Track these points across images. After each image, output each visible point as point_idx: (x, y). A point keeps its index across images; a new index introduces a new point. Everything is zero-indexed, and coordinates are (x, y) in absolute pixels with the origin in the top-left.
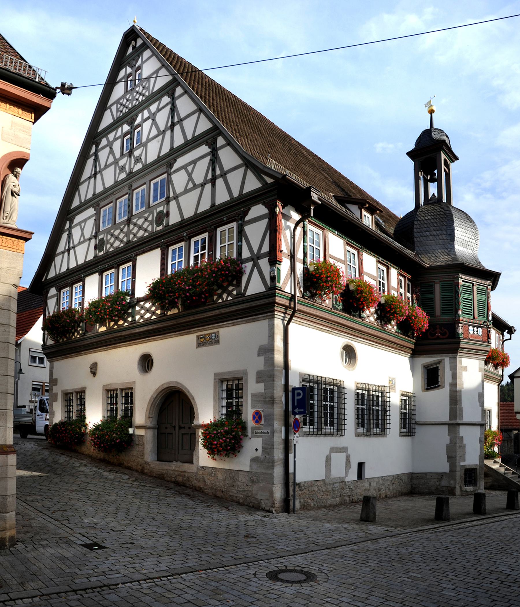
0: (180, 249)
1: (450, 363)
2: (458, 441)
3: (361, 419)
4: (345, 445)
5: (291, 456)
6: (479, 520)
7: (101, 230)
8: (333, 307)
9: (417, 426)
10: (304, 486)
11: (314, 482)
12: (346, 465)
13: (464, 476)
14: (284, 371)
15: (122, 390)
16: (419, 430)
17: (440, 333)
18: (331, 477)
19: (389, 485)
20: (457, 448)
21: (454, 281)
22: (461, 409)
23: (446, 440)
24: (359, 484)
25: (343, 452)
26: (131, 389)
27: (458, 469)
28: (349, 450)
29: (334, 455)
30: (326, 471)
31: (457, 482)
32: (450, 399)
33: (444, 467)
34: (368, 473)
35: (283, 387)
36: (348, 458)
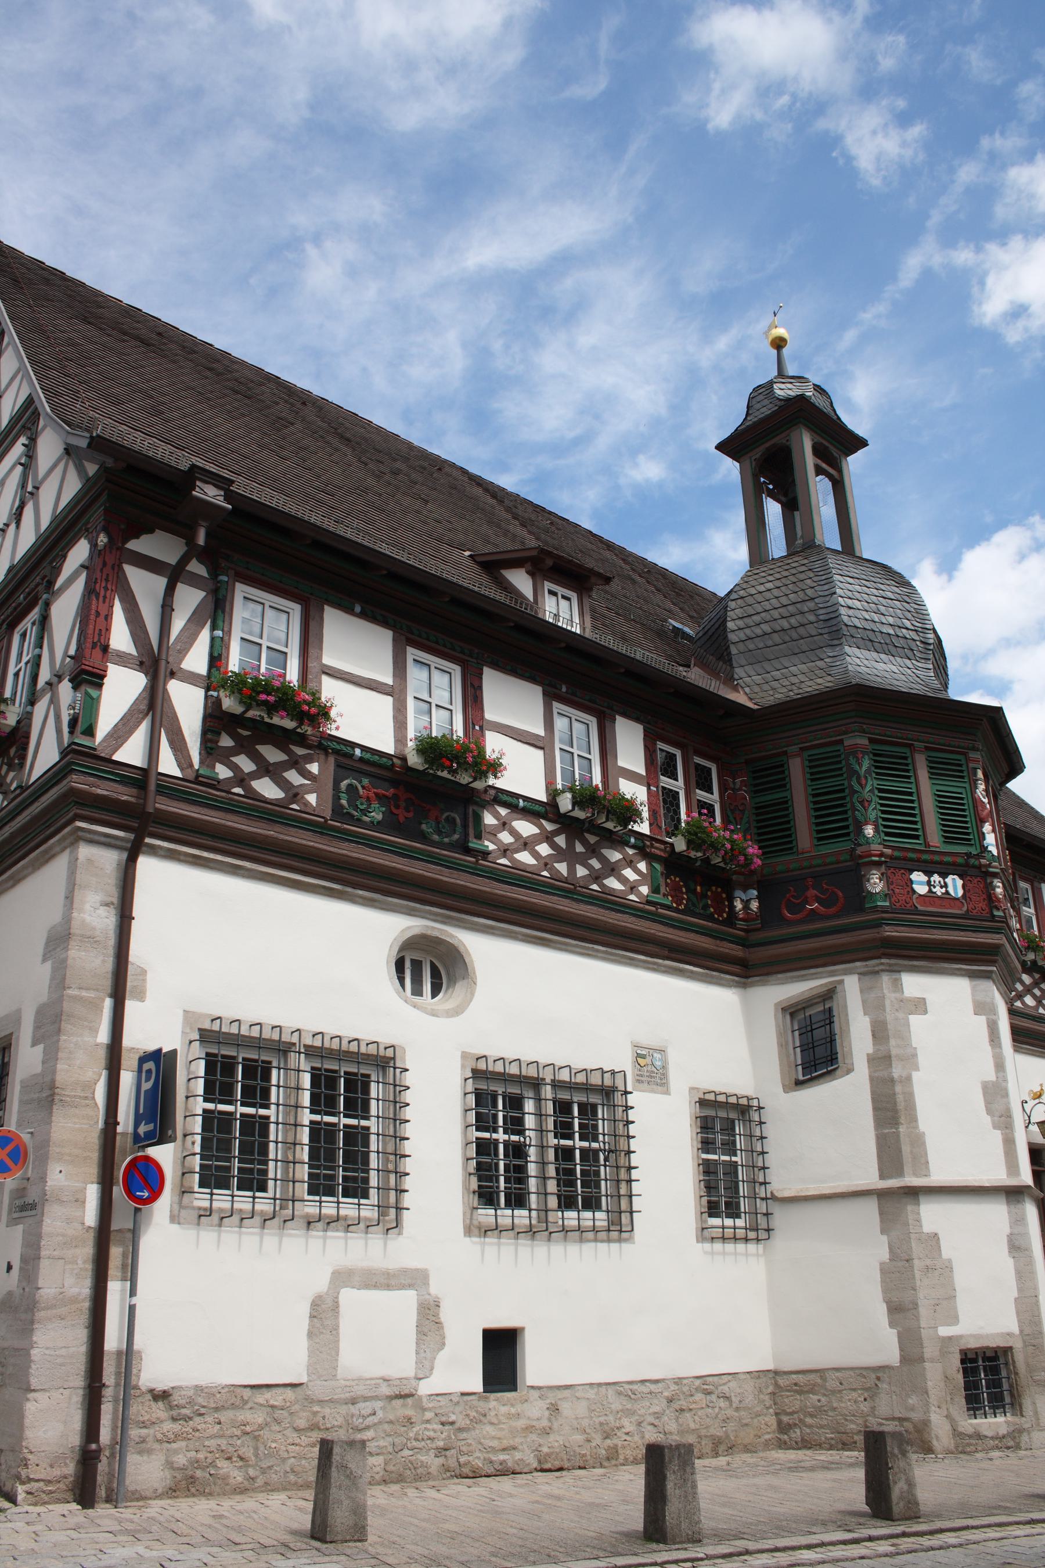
1: (861, 991)
2: (917, 1249)
3: (496, 1180)
5: (115, 1289)
6: (844, 1542)
8: (338, 811)
9: (775, 1208)
10: (191, 1402)
11: (247, 1393)
12: (421, 1333)
13: (960, 1378)
14: (108, 1003)
16: (781, 1217)
17: (818, 899)
18: (340, 1373)
19: (658, 1415)
20: (918, 1274)
21: (841, 742)
22: (919, 1141)
23: (880, 1250)
24: (500, 1403)
25: (410, 1286)
27: (930, 1350)
28: (432, 1282)
29: (348, 1297)
31: (933, 1399)
32: (875, 1109)
33: (883, 1346)
34: (536, 1365)
35: (102, 1054)
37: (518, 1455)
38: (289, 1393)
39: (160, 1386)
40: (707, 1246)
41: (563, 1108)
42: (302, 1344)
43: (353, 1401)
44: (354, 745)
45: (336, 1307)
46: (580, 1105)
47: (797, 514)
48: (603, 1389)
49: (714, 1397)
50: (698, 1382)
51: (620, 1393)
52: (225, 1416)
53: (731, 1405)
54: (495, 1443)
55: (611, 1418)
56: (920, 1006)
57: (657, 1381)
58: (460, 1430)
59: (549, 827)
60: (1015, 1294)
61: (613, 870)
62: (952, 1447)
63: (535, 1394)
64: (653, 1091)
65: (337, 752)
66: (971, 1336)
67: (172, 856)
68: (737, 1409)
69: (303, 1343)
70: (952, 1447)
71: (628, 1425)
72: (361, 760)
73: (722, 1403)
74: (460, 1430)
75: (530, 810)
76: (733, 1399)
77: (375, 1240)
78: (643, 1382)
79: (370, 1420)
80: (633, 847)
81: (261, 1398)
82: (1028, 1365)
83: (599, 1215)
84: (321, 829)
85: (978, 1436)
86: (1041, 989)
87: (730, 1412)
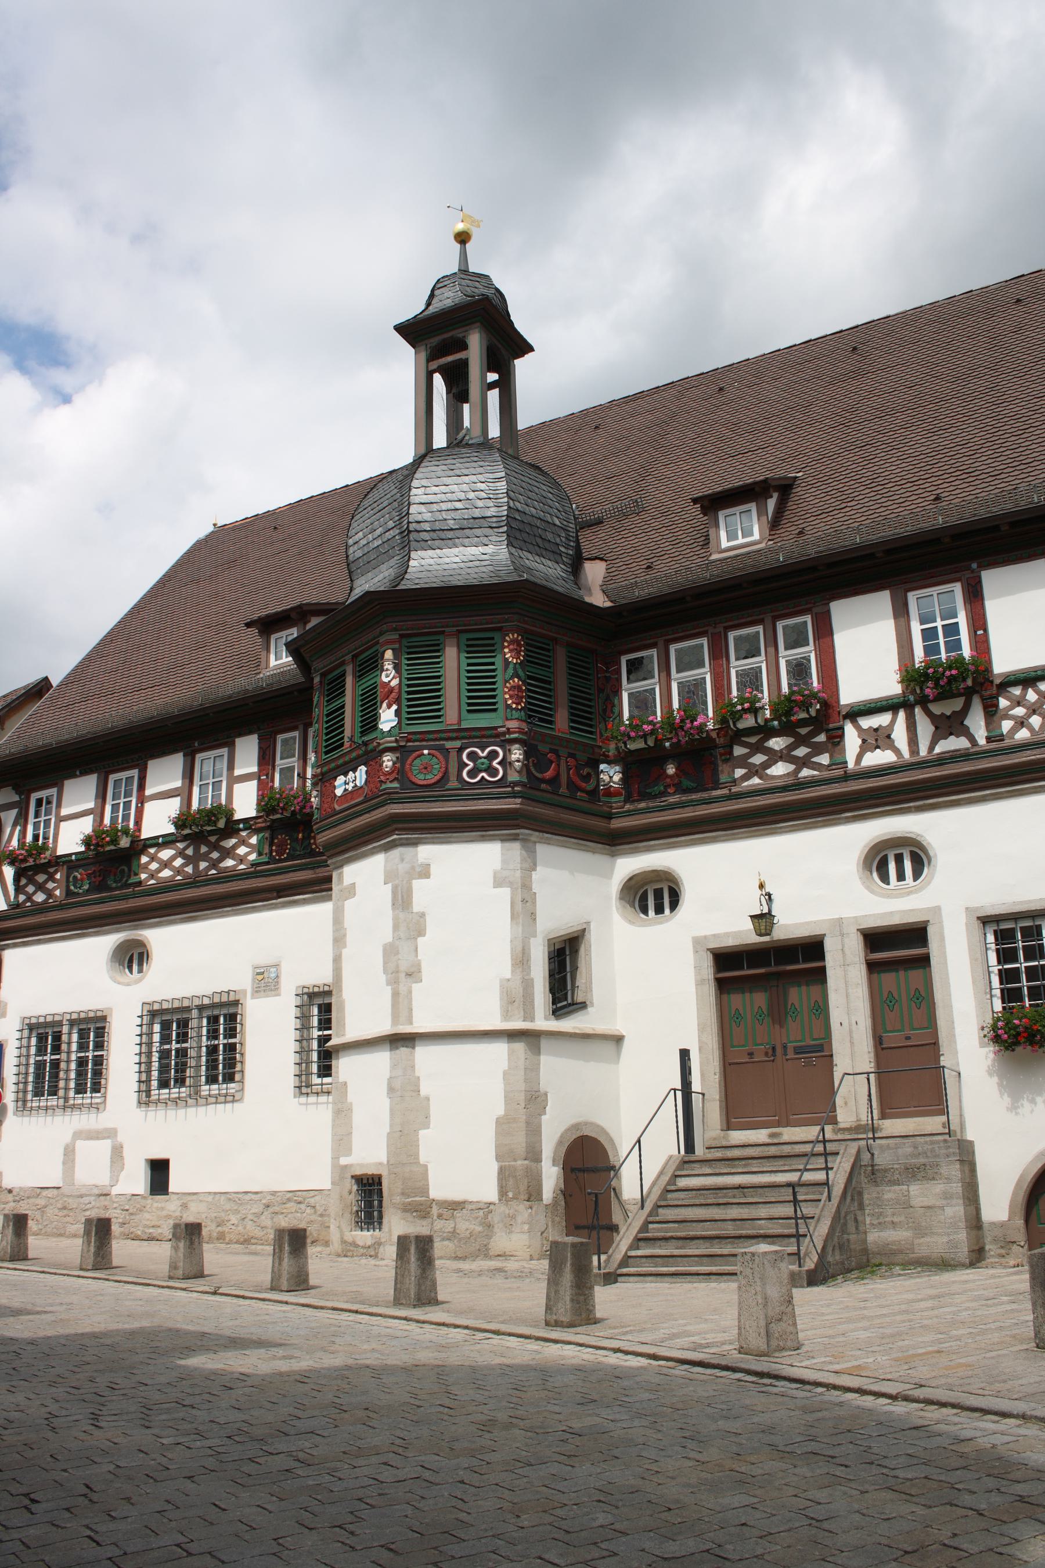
0: (129, 780)
4: (110, 1125)
7: (271, 665)
11: (39, 1191)
15: (72, 1023)
18: (76, 1182)
25: (108, 1137)
26: (236, 1003)
29: (79, 1144)
30: (65, 1172)
36: (117, 1153)
37: (160, 1231)
38: (55, 1191)
39: (9, 1187)
40: (303, 1099)
41: (214, 1020)
42: (59, 1167)
43: (81, 1196)
44: (70, 855)
45: (73, 1150)
46: (225, 1016)
47: (466, 407)
48: (218, 1196)
49: (303, 1206)
50: (290, 1195)
51: (230, 1199)
52: (31, 1201)
53: (315, 1212)
54: (148, 1223)
55: (223, 1214)
56: (425, 873)
57: (256, 1193)
58: (132, 1214)
59: (181, 845)
60: (388, 1130)
61: (228, 854)
62: (340, 1251)
63: (175, 1197)
64: (267, 996)
65: (64, 863)
66: (358, 1165)
67: (15, 946)
68: (321, 1215)
69: (61, 1166)
70: (340, 1251)
71: (234, 1219)
72: (77, 860)
73: (309, 1210)
74: (132, 1214)
75: (167, 841)
76: (318, 1207)
77: (93, 1116)
78: (246, 1193)
79: (88, 1206)
80: (245, 829)
81: (45, 1193)
82: (390, 1189)
83: (183, 1089)
84: (61, 907)
85: (355, 1244)
86: (1038, 692)
87: (313, 1217)
